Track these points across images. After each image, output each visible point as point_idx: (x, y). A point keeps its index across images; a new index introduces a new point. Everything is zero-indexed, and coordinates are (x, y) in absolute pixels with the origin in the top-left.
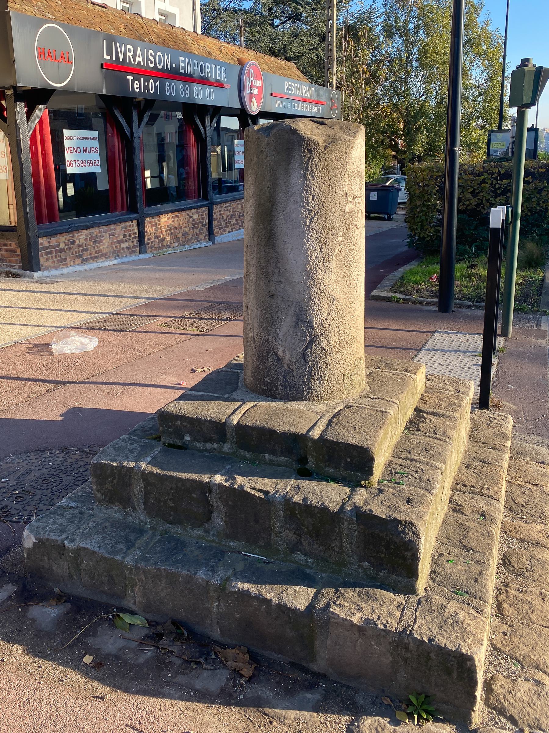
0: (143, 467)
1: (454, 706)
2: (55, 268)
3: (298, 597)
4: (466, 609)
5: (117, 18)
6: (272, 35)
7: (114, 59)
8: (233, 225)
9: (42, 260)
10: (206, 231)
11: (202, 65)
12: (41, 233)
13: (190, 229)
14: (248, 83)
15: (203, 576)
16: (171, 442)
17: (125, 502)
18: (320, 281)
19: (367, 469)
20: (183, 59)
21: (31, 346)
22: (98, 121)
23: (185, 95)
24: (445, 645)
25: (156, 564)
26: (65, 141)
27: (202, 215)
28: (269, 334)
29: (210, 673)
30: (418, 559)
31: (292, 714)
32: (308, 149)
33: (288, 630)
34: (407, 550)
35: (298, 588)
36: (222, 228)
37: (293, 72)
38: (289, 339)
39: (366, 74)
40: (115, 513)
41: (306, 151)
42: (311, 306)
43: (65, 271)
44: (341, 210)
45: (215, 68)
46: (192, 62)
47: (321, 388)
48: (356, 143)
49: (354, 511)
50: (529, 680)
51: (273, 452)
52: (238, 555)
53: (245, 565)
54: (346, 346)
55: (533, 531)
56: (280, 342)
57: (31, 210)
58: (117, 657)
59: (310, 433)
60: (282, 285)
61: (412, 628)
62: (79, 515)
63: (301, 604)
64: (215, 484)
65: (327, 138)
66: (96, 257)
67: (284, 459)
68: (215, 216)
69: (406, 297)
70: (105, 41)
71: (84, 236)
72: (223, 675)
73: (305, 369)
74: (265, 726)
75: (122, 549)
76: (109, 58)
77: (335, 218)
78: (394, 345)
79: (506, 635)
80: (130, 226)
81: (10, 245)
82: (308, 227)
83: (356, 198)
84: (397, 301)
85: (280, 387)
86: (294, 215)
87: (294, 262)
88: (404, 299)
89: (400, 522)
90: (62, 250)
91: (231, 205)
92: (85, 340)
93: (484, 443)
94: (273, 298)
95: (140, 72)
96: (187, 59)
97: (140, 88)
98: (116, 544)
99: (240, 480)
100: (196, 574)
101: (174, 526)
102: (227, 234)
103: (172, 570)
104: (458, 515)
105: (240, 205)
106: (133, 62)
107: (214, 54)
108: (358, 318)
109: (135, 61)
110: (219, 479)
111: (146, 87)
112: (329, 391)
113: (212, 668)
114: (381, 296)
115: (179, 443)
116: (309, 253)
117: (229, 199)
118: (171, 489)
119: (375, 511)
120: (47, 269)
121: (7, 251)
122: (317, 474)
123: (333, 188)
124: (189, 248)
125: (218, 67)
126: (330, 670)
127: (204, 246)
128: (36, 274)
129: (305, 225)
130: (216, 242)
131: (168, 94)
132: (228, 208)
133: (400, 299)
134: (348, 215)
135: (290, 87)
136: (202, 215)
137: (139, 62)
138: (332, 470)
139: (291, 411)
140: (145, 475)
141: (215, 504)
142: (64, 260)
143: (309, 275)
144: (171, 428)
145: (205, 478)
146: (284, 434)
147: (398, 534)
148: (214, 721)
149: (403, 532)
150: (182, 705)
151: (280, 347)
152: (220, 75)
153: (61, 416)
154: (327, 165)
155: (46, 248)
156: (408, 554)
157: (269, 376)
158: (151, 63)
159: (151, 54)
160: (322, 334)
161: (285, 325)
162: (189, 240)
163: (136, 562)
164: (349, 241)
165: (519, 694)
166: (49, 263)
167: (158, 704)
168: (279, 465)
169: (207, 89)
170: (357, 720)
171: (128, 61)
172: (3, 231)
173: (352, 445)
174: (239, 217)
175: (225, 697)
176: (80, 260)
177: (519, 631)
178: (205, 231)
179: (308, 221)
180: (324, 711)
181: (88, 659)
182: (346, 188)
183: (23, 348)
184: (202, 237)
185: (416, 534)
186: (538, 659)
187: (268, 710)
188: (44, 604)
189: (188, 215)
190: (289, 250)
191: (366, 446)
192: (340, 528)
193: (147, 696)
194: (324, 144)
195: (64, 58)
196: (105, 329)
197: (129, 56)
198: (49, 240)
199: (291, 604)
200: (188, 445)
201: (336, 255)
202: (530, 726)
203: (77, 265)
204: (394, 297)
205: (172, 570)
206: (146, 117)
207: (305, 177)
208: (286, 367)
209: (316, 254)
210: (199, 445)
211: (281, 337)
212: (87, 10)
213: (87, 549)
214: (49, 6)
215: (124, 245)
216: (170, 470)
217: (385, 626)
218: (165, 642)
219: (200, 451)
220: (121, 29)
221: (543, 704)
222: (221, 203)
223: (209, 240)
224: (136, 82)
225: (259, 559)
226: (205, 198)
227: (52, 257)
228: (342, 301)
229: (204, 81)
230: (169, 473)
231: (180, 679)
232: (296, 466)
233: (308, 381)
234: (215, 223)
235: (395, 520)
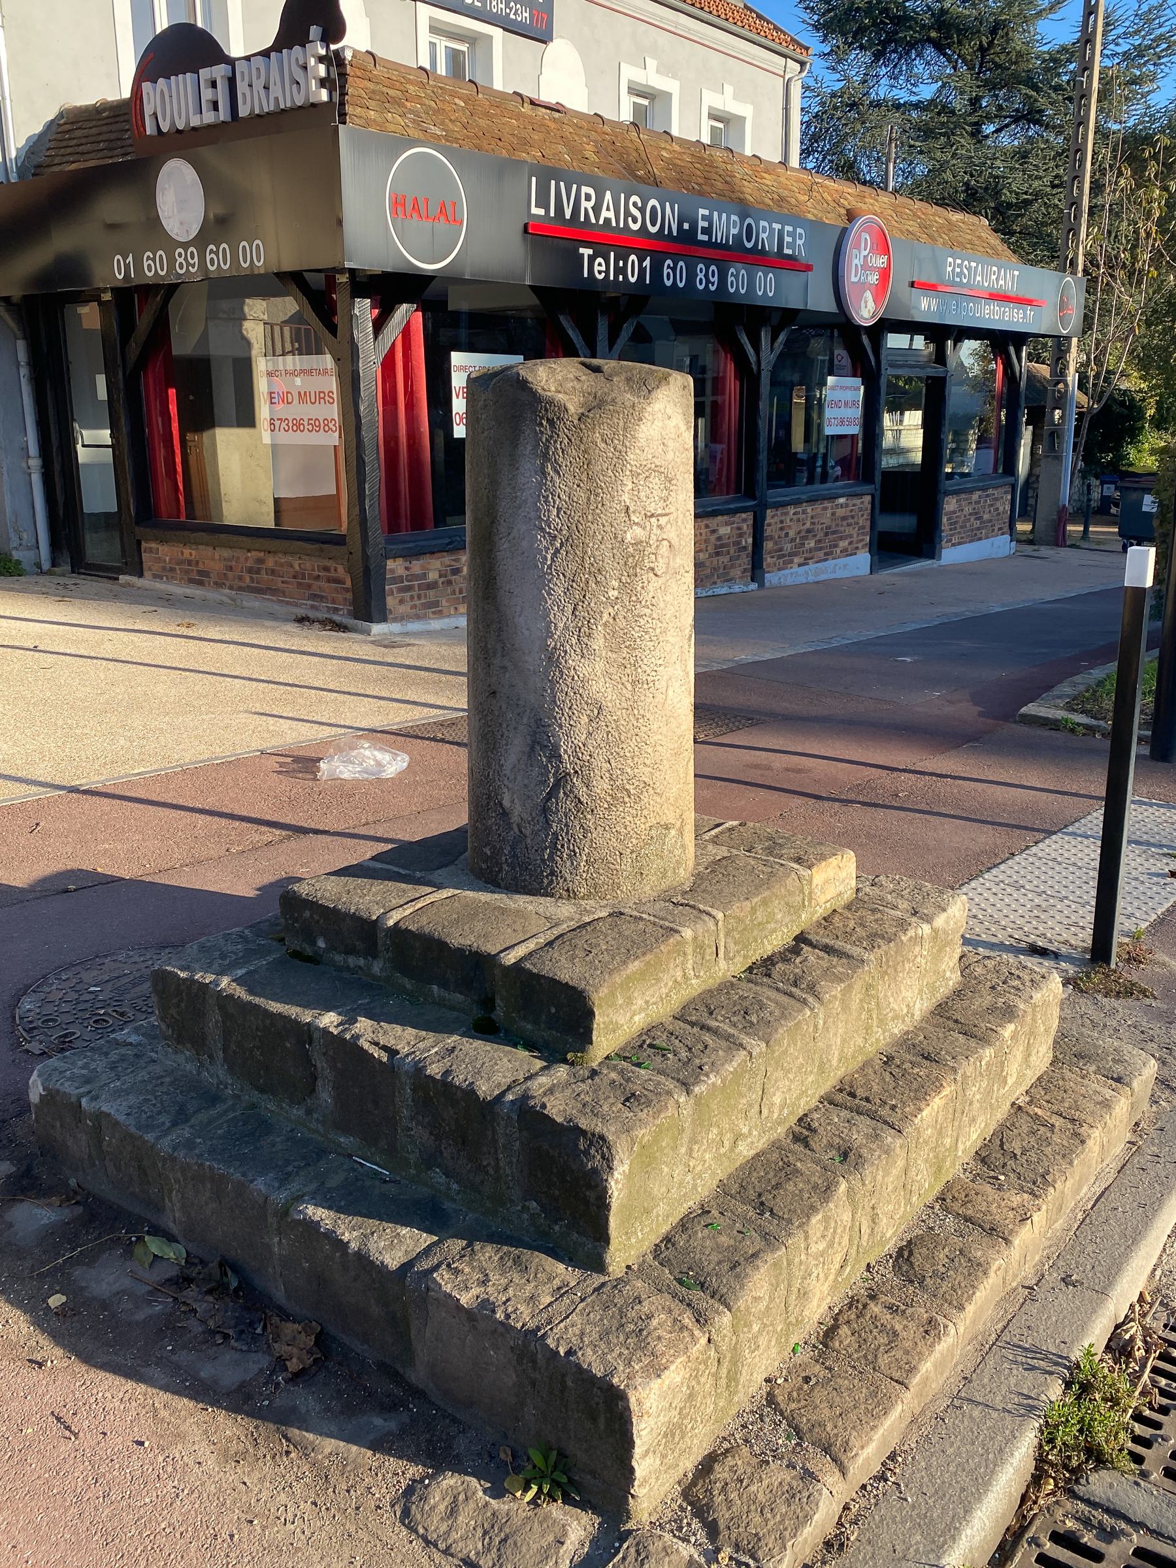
0: (222, 985)
1: (604, 1481)
2: (418, 617)
3: (394, 1245)
4: (676, 1313)
5: (582, 132)
6: (971, 157)
7: (552, 214)
8: (811, 550)
9: (391, 602)
10: (746, 561)
11: (749, 225)
12: (391, 550)
13: (710, 556)
14: (856, 261)
15: (262, 1187)
16: (298, 948)
17: (198, 1043)
18: (573, 672)
19: (582, 1030)
20: (706, 212)
21: (289, 760)
23: (707, 285)
24: (590, 1364)
25: (201, 1156)
26: (453, 373)
27: (739, 528)
28: (489, 765)
29: (237, 1355)
30: (608, 1207)
31: (330, 1445)
32: (548, 420)
33: (372, 1301)
34: (590, 1187)
35: (404, 1231)
36: (784, 556)
37: (979, 237)
38: (519, 778)
39: (1155, 240)
40: (183, 1061)
41: (544, 423)
42: (555, 718)
43: (436, 624)
44: (616, 538)
45: (781, 233)
46: (728, 219)
47: (577, 874)
48: (649, 409)
49: (519, 1104)
50: (794, 1468)
51: (444, 985)
52: (347, 1160)
53: (346, 1179)
54: (627, 799)
55: (999, 1206)
56: (506, 782)
57: (375, 506)
58: (104, 1305)
59: (502, 955)
60: (507, 675)
61: (551, 1329)
62: (132, 1059)
63: (393, 1260)
64: (318, 1028)
65: (591, 398)
67: (459, 997)
68: (768, 531)
69: (1094, 722)
70: (534, 179)
72: (259, 1362)
73: (547, 837)
74: (274, 1458)
75: (163, 1123)
76: (542, 212)
77: (603, 552)
78: (1005, 818)
79: (807, 1383)
81: (335, 570)
82: (550, 567)
83: (652, 516)
84: (1072, 731)
85: (505, 867)
86: (524, 544)
87: (526, 633)
88: (1087, 727)
89: (584, 1133)
90: (432, 586)
91: (809, 510)
92: (384, 757)
93: (956, 1021)
94: (495, 697)
95: (608, 242)
96: (716, 214)
97: (607, 272)
98: (159, 1113)
99: (363, 1025)
100: (252, 1181)
101: (265, 1097)
102: (795, 569)
103: (220, 1168)
104: (798, 1148)
105: (829, 512)
106: (593, 221)
107: (793, 201)
108: (659, 748)
109: (597, 218)
110: (329, 1020)
111: (623, 271)
112: (590, 882)
113: (244, 1348)
114: (1041, 717)
115: (309, 951)
116: (552, 616)
117: (804, 497)
118: (257, 1029)
119: (549, 1108)
120: (401, 619)
121: (329, 580)
122: (506, 1031)
123: (597, 495)
124: (704, 594)
125: (788, 228)
126: (431, 1385)
127: (737, 590)
128: (377, 629)
129: (543, 563)
130: (767, 584)
131: (668, 283)
132: (801, 516)
133: (1079, 724)
134: (631, 550)
135: (958, 270)
136: (739, 528)
137: (607, 220)
138: (529, 1027)
139: (503, 911)
140: (226, 1001)
141: (319, 1065)
142: (436, 604)
143: (553, 659)
144: (297, 921)
145: (307, 1016)
146: (460, 951)
147: (576, 1153)
148: (196, 1433)
149: (586, 1153)
150: (161, 1398)
151: (505, 790)
152: (791, 246)
153: (258, 889)
154: (585, 452)
155: (400, 579)
156: (591, 1195)
157: (488, 844)
158: (635, 221)
159: (635, 204)
160: (576, 772)
161: (513, 751)
162: (707, 577)
163: (175, 1149)
164: (634, 598)
165: (753, 1488)
166: (403, 609)
167: (123, 1389)
168: (452, 1008)
169: (760, 274)
170: (431, 1477)
171: (582, 219)
172: (323, 543)
173: (559, 982)
174: (826, 534)
175: (238, 1400)
177: (838, 1380)
178: (745, 561)
179: (549, 556)
180: (388, 1452)
181: (56, 1301)
182: (625, 497)
183: (272, 763)
184: (736, 572)
185: (608, 1161)
186: (836, 1435)
187: (294, 1433)
188: (42, 1201)
189: (707, 526)
190: (518, 609)
191: (583, 986)
192: (494, 1131)
193: (115, 1373)
194: (580, 411)
195: (447, 213)
196: (442, 741)
197: (586, 209)
198: (407, 564)
199: (377, 1255)
200: (321, 956)
201: (605, 625)
202: (737, 1547)
204: (1066, 721)
205: (220, 1168)
206: (627, 330)
207: (544, 474)
208: (516, 830)
209: (565, 619)
210: (339, 958)
211: (508, 772)
212: (518, 116)
213: (109, 1115)
214: (438, 111)
216: (260, 996)
217: (508, 1316)
218: (191, 1293)
219: (339, 969)
220: (588, 154)
221: (790, 1514)
222: (784, 505)
223: (753, 580)
224: (600, 260)
225: (376, 1173)
226: (750, 494)
227: (412, 598)
228: (619, 713)
229: (758, 258)
230: (257, 1000)
231: (184, 1357)
232: (477, 1013)
233: (551, 858)
234: (768, 545)
235: (577, 1128)
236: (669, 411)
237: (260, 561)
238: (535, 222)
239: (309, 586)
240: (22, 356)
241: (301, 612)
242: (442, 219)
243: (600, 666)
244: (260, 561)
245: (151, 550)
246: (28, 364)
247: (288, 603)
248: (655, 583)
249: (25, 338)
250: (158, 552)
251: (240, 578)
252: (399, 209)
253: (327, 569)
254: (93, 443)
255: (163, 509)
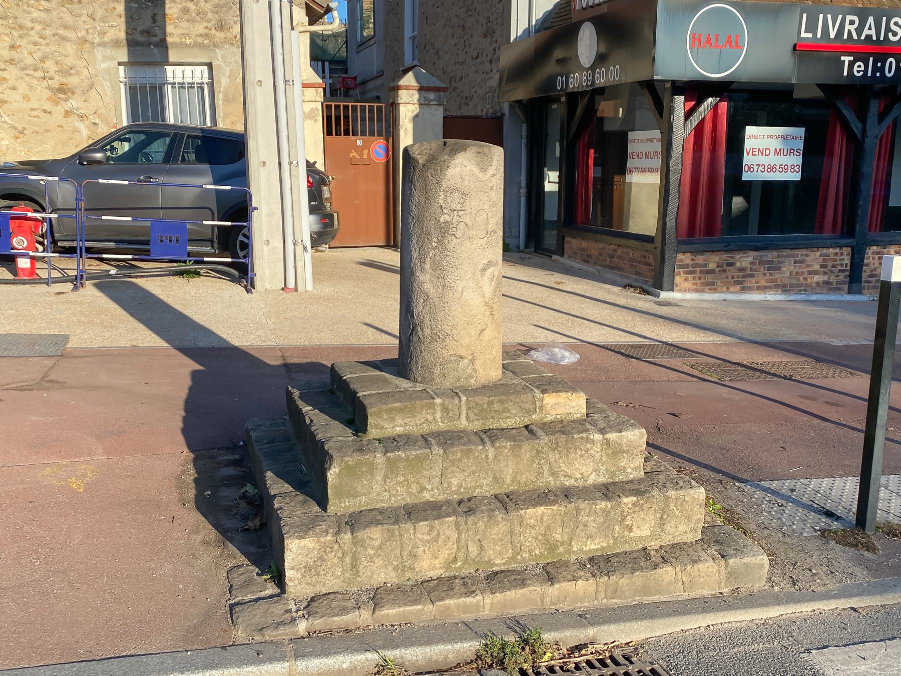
9: (678, 279)
22: (517, 131)
66: (766, 288)
70: (805, 15)
71: (751, 259)
80: (836, 254)
90: (712, 272)
109: (859, 35)
142: (713, 284)
176: (738, 287)
182: (441, 201)
197: (850, 31)
198: (693, 257)
203: (732, 292)
215: (817, 278)
236: (465, 163)
237: (615, 251)
238: (803, 42)
239: (636, 266)
240: (524, 133)
241: (628, 282)
242: (728, 46)
243: (428, 277)
244: (615, 251)
245: (568, 242)
246: (527, 137)
247: (625, 276)
248: (455, 241)
249: (527, 122)
250: (573, 243)
251: (605, 260)
252: (696, 43)
253: (645, 257)
254: (551, 182)
255: (579, 218)
